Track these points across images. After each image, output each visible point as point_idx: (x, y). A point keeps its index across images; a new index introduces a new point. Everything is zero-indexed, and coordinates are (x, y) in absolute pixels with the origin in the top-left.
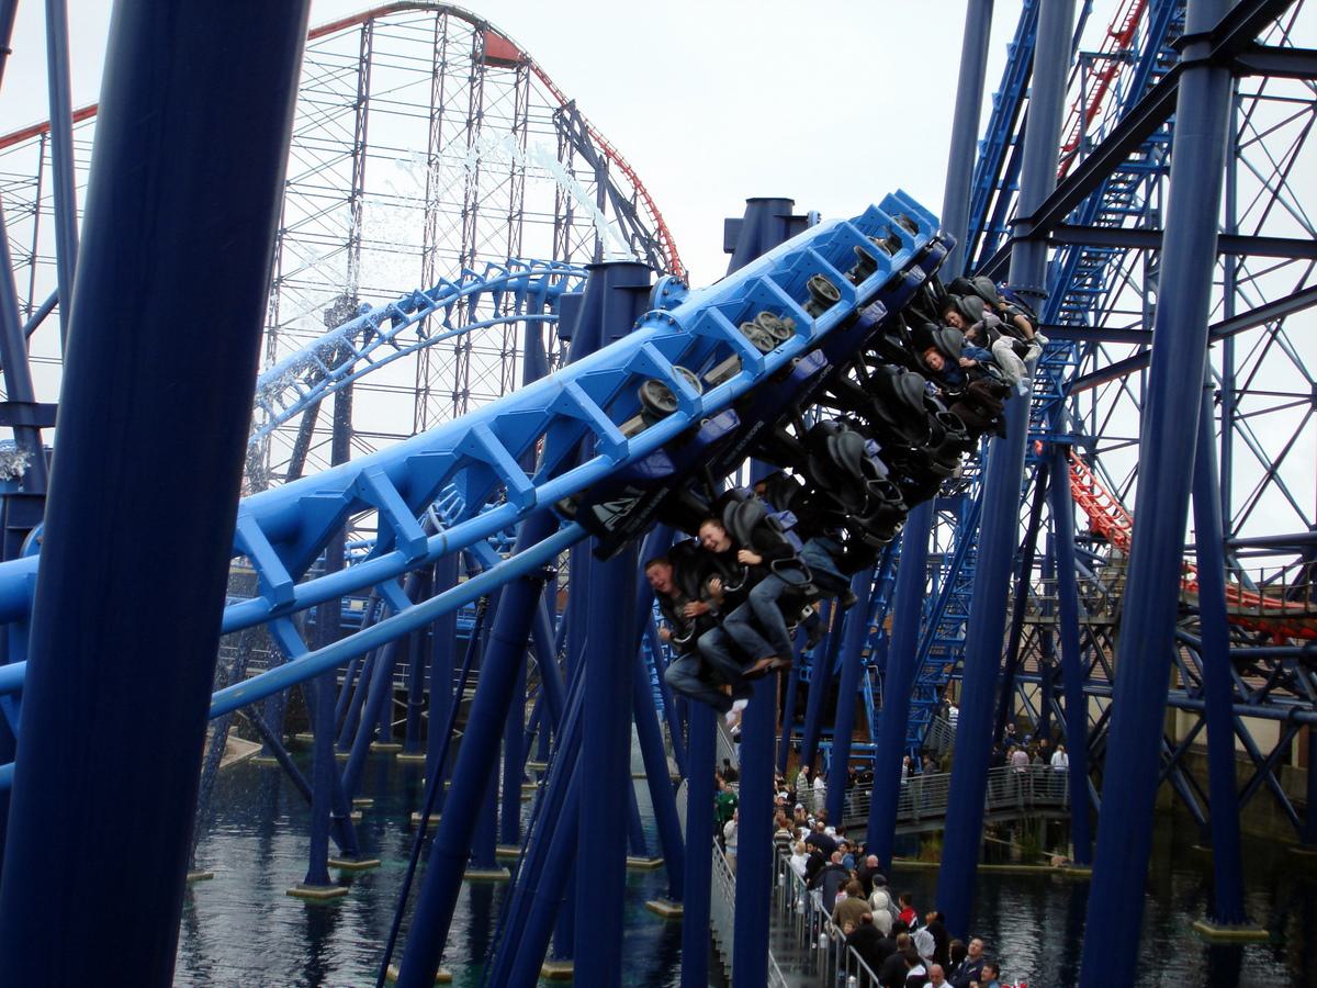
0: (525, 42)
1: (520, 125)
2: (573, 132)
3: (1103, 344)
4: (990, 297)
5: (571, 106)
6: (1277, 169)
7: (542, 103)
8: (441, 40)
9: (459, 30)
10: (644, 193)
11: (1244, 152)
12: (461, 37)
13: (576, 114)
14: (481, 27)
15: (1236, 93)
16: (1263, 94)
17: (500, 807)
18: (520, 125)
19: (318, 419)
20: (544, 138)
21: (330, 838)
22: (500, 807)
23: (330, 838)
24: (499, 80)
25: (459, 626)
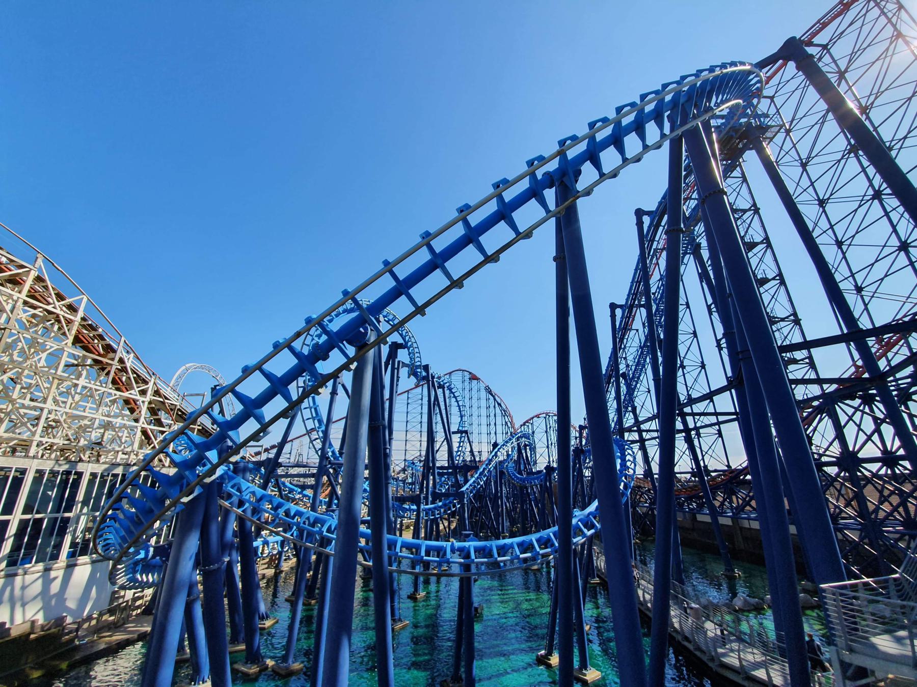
0: (478, 376)
1: (479, 390)
2: (489, 391)
3: (882, 369)
4: (450, 578)
5: (488, 386)
6: (776, 300)
7: (482, 386)
8: (463, 376)
9: (466, 374)
10: (499, 405)
11: (818, 207)
12: (467, 376)
13: (489, 388)
14: (470, 373)
15: (548, 629)
16: (813, 181)
17: (774, 433)
18: (479, 390)
19: (811, 378)
20: (483, 394)
21: (597, 500)
22: (774, 433)
23: (597, 500)
24: (475, 382)
25: (799, 397)
